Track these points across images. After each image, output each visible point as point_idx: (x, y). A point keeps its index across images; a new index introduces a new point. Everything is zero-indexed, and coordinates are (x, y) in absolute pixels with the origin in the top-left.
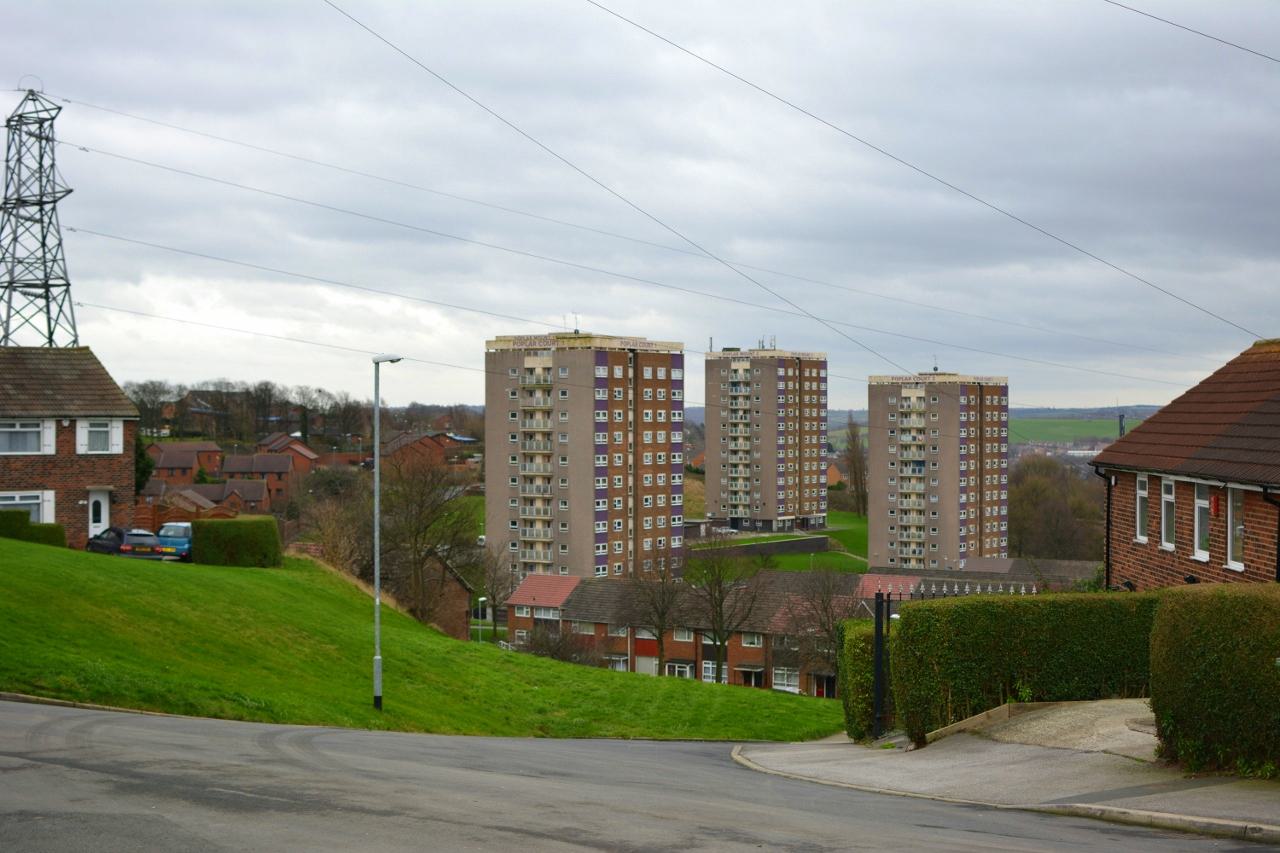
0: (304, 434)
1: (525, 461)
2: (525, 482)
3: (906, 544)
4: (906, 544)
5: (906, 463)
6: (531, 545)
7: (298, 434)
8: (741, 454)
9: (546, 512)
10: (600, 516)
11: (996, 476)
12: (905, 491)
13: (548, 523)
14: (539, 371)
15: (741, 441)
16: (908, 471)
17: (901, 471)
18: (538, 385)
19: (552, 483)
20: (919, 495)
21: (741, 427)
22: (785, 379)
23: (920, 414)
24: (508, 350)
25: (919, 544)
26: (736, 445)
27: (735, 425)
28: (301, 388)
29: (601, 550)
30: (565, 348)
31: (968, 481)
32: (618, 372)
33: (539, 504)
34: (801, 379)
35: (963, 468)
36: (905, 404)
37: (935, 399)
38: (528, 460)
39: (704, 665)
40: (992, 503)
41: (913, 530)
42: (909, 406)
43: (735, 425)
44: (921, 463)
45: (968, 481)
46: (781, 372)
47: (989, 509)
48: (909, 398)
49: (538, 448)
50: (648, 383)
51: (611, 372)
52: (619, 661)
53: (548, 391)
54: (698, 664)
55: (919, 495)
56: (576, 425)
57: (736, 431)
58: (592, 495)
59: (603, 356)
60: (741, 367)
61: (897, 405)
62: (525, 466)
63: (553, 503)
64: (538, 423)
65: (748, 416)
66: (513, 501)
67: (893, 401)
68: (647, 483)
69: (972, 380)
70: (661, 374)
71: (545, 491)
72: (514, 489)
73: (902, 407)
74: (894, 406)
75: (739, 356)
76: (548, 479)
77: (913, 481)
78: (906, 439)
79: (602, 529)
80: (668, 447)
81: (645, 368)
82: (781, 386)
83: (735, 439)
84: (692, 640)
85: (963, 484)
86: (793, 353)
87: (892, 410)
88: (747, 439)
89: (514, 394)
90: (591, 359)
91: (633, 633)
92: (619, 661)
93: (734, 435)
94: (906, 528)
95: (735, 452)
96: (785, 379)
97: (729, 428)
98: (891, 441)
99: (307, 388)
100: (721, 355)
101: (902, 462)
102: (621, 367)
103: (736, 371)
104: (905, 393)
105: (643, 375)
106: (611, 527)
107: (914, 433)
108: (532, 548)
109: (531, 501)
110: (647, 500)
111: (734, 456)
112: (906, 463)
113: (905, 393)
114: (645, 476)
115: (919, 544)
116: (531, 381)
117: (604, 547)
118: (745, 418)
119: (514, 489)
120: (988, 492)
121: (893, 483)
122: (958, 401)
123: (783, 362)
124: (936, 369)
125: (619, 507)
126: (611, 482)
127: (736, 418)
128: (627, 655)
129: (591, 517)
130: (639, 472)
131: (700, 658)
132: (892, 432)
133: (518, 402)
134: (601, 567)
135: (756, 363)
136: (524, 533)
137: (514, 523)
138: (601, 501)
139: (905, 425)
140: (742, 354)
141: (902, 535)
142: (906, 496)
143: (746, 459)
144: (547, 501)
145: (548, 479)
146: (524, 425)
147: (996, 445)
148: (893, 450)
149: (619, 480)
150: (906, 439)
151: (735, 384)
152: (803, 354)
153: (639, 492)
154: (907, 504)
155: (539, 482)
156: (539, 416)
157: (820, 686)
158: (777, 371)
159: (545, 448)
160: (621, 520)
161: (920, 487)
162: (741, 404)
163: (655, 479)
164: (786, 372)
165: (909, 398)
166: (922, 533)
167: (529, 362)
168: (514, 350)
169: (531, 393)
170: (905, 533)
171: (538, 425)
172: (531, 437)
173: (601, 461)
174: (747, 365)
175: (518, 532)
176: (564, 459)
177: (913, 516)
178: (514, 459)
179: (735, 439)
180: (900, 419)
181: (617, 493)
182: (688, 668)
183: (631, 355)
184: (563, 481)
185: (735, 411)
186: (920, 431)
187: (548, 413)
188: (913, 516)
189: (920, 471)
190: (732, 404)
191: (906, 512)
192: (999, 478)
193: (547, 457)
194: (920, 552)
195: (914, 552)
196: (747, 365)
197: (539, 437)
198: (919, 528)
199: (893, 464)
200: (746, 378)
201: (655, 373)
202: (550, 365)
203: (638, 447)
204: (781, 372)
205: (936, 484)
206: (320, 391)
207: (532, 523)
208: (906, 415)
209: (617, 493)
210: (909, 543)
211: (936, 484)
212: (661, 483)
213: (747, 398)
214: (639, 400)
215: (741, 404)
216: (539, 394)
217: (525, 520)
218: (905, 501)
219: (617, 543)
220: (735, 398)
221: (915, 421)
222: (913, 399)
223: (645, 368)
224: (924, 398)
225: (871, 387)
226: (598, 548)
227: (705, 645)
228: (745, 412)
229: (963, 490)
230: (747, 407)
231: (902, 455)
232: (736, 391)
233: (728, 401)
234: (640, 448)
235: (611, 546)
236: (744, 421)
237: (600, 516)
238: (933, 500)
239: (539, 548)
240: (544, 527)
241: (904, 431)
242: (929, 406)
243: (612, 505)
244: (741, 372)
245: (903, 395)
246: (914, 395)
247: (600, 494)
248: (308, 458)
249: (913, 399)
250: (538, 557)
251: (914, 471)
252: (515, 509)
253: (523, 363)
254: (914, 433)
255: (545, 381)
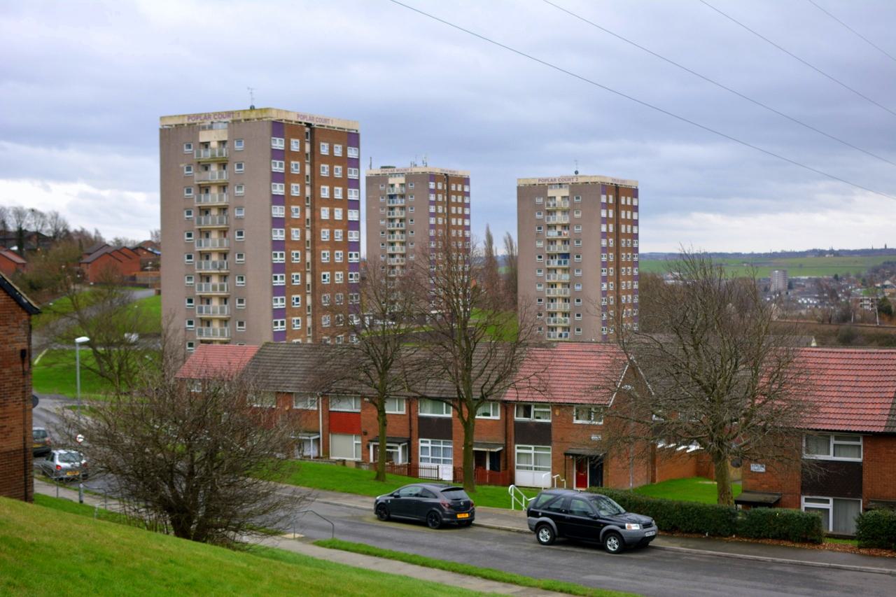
0: (20, 249)
1: (201, 237)
2: (201, 258)
3: (553, 329)
4: (553, 329)
5: (552, 256)
6: (208, 322)
7: (15, 248)
8: (397, 257)
9: (222, 289)
10: (278, 291)
11: (629, 268)
12: (552, 280)
13: (224, 300)
14: (214, 144)
15: (397, 246)
16: (554, 263)
17: (548, 263)
18: (214, 160)
19: (229, 257)
20: (564, 284)
21: (397, 233)
22: (435, 191)
23: (564, 212)
24: (183, 125)
25: (564, 328)
26: (393, 249)
27: (392, 232)
28: (16, 208)
29: (279, 326)
30: (240, 120)
31: (608, 272)
32: (295, 146)
33: (215, 281)
34: (448, 192)
35: (604, 259)
36: (551, 203)
37: (578, 198)
38: (204, 235)
39: (421, 445)
40: (627, 292)
41: (559, 316)
42: (555, 205)
43: (392, 232)
44: (566, 256)
45: (608, 272)
46: (432, 185)
47: (624, 297)
48: (555, 197)
49: (214, 223)
50: (325, 159)
51: (288, 144)
52: (309, 441)
53: (223, 165)
54: (413, 443)
55: (564, 284)
56: (254, 199)
57: (393, 238)
58: (269, 269)
59: (279, 128)
60: (397, 181)
61: (544, 204)
62: (201, 242)
63: (229, 279)
64: (214, 198)
65: (404, 224)
66: (189, 278)
67: (539, 200)
68: (325, 260)
69: (610, 182)
70: (338, 152)
71: (221, 267)
72: (190, 266)
73: (549, 205)
74: (542, 205)
75: (396, 172)
76: (224, 255)
77: (559, 272)
78: (553, 234)
79: (279, 304)
80: (345, 224)
81: (322, 144)
82: (432, 198)
83: (392, 244)
84: (404, 412)
85: (604, 274)
86: (442, 170)
87: (539, 208)
88: (403, 244)
89: (189, 169)
90: (268, 129)
91: (326, 405)
92: (309, 441)
93: (391, 240)
94: (552, 314)
95: (392, 256)
96: (435, 191)
97: (387, 235)
98: (539, 237)
99: (22, 208)
100: (380, 172)
101: (548, 255)
102: (298, 141)
103: (392, 186)
104: (550, 193)
105: (319, 151)
106: (289, 302)
107: (559, 229)
108: (208, 325)
109: (207, 278)
110: (324, 277)
111: (391, 259)
112: (552, 256)
113: (550, 193)
114: (323, 252)
115: (564, 328)
116: (205, 155)
117: (282, 323)
118: (402, 226)
119: (190, 266)
120: (624, 282)
121: (541, 274)
122: (600, 198)
123: (433, 177)
124: (576, 172)
125: (297, 282)
126: (289, 257)
127: (393, 226)
128: (319, 433)
129: (269, 292)
130: (317, 247)
131: (415, 433)
132: (540, 228)
133: (193, 177)
134: (279, 321)
135: (410, 178)
136: (201, 311)
137: (190, 301)
138: (278, 275)
139: (552, 222)
140: (397, 171)
141: (549, 320)
142: (553, 285)
143: (402, 261)
144: (224, 277)
145: (224, 255)
146: (199, 200)
147: (629, 240)
148: (540, 245)
149: (297, 254)
150: (553, 234)
151: (391, 197)
152: (450, 171)
153: (317, 268)
154: (554, 292)
155: (215, 258)
156: (214, 190)
157: (580, 468)
158: (429, 185)
159: (221, 223)
160: (299, 296)
161: (566, 277)
162: (398, 214)
163: (332, 256)
164: (436, 186)
165: (555, 197)
166: (567, 318)
167: (204, 136)
168: (189, 125)
169: (206, 168)
170: (552, 319)
171: (214, 200)
172: (207, 212)
173: (278, 258)
174: (402, 180)
175: (194, 309)
176: (240, 234)
177: (559, 303)
178: (189, 235)
179: (392, 244)
180: (546, 217)
181: (295, 268)
182: (400, 450)
183: (307, 129)
184: (240, 256)
185: (392, 220)
186: (565, 226)
187: (223, 187)
188: (559, 303)
189: (565, 263)
190: (389, 214)
191: (552, 300)
192: (632, 270)
193: (224, 232)
194: (566, 336)
195: (561, 335)
196: (402, 180)
197: (214, 212)
198: (565, 314)
199: (540, 257)
200: (402, 191)
201: (331, 149)
202: (226, 139)
203: (315, 223)
204: (432, 185)
205: (579, 274)
206: (33, 210)
207: (208, 300)
208: (550, 212)
209: (295, 268)
210: (556, 328)
211: (579, 274)
212: (338, 260)
213: (402, 208)
214: (316, 176)
215: (398, 214)
216: (214, 168)
217: (202, 298)
218: (552, 290)
219: (295, 319)
220: (392, 208)
221: (559, 218)
222: (559, 199)
223: (322, 144)
224: (568, 197)
225: (519, 188)
226: (276, 324)
227: (421, 419)
228: (401, 220)
229: (605, 279)
230: (403, 216)
231: (548, 249)
232: (393, 202)
233: (385, 211)
234: (317, 224)
235: (289, 323)
236: (400, 228)
237: (278, 291)
238: (578, 288)
239: (216, 325)
240: (220, 303)
241: (549, 227)
242: (573, 204)
243: (289, 281)
244: (397, 186)
245: (549, 195)
246: (558, 194)
247: (277, 268)
248: (14, 261)
249: (559, 199)
250: (215, 334)
251: (560, 263)
252: (191, 287)
253: (198, 137)
254: (559, 229)
255: (221, 154)
